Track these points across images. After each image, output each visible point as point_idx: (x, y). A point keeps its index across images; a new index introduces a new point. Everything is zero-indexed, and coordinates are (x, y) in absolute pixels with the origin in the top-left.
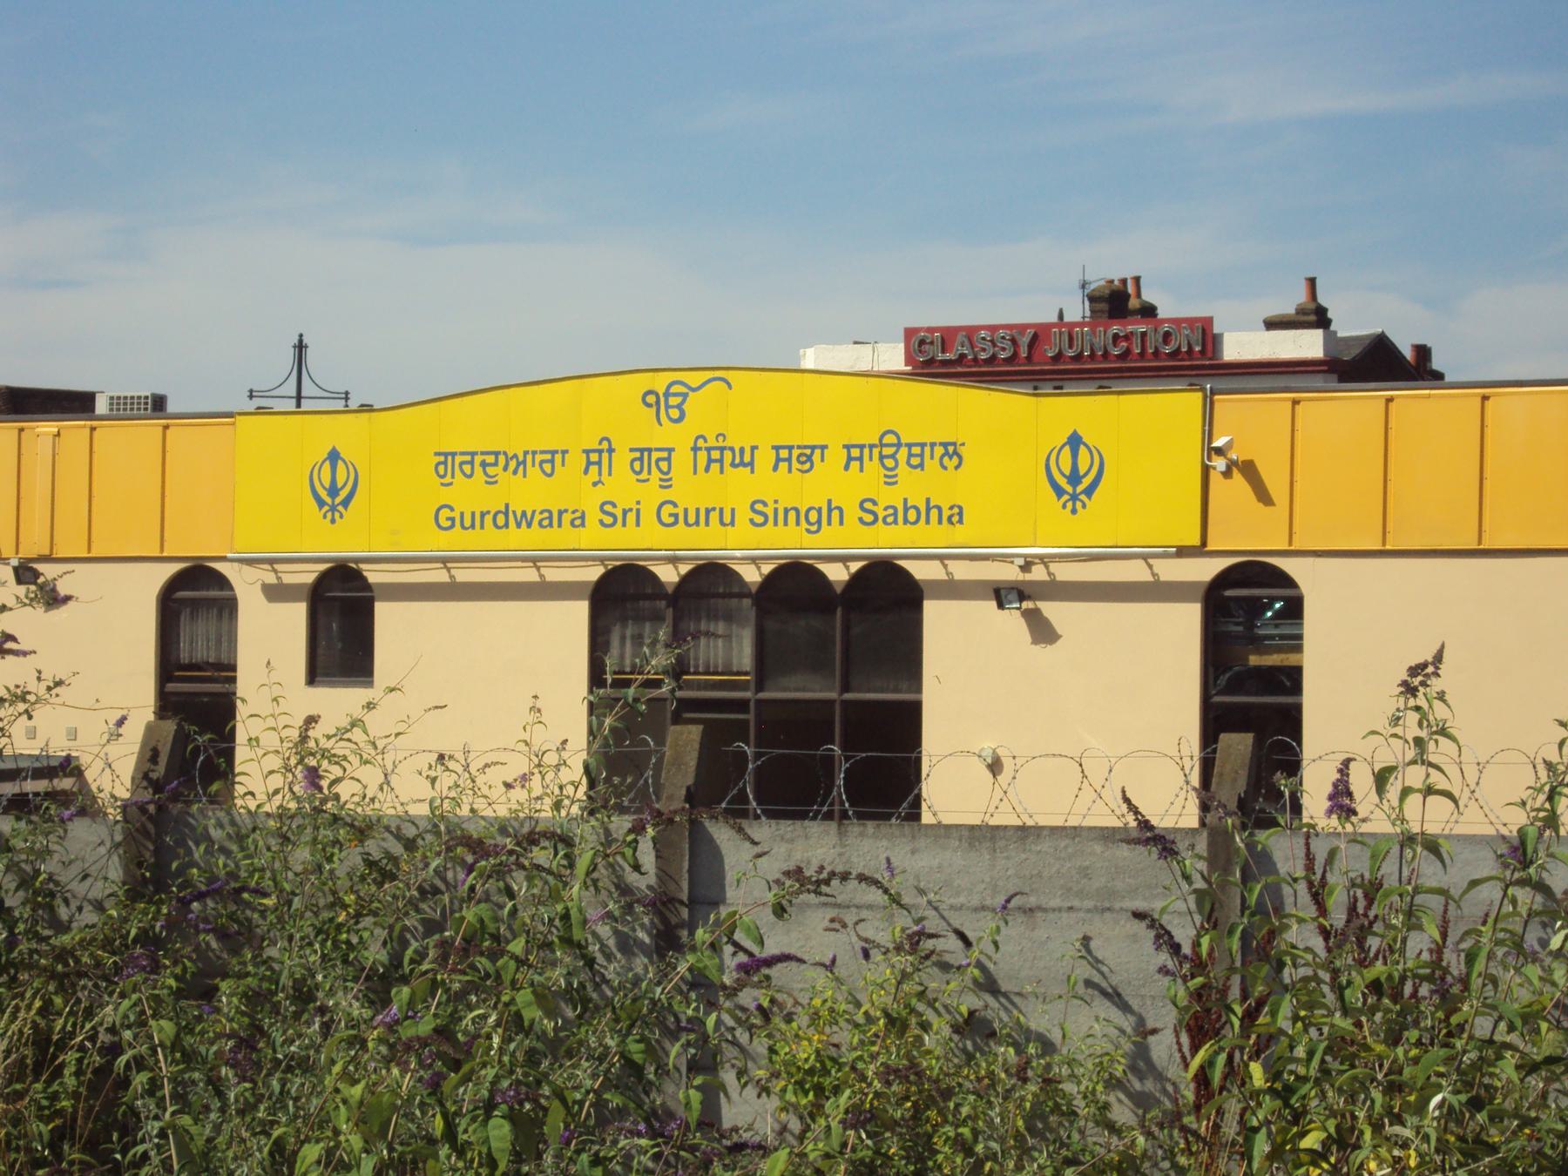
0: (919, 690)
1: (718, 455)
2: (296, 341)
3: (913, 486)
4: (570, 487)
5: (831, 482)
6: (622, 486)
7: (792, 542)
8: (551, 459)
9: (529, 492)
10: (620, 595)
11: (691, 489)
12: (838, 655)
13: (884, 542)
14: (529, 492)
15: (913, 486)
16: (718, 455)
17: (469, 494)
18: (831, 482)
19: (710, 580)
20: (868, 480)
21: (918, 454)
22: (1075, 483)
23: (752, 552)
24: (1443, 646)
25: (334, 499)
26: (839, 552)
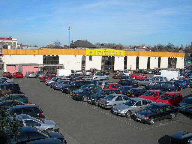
0: (85, 66)
1: (107, 52)
2: (37, 46)
3: (115, 53)
4: (101, 53)
5: (112, 53)
6: (104, 53)
7: (110, 55)
8: (101, 52)
9: (100, 53)
10: (103, 57)
11: (106, 53)
12: (52, 65)
13: (113, 55)
14: (100, 53)
15: (115, 53)
16: (107, 52)
17: (97, 53)
18: (112, 53)
19: (107, 56)
20: (113, 53)
21: (115, 52)
22: (120, 53)
23: (108, 55)
24: (182, 44)
25: (91, 53)
26: (112, 55)
